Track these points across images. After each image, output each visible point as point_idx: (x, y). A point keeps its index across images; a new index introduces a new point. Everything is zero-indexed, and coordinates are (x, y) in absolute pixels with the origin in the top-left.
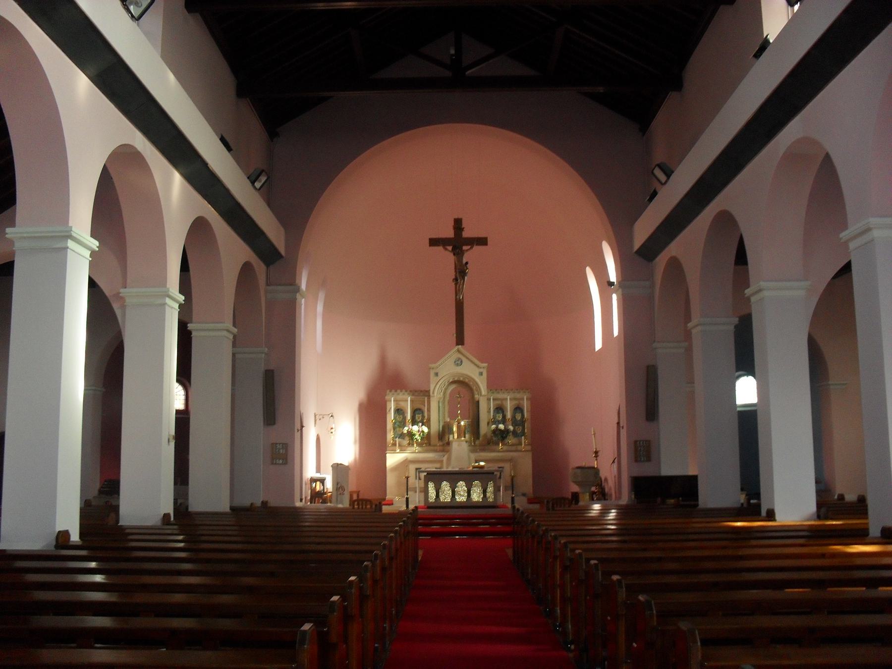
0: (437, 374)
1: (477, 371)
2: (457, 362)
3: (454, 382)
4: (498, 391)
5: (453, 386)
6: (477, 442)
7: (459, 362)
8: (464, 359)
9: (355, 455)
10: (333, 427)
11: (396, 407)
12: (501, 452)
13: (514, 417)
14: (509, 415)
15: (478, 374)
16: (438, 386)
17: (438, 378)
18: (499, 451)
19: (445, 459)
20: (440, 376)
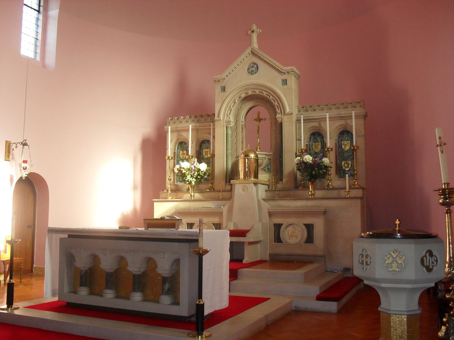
0: (224, 89)
1: (280, 78)
2: (251, 69)
3: (247, 98)
4: (321, 107)
5: (249, 105)
6: (280, 186)
7: (254, 69)
8: (261, 64)
9: (135, 204)
10: (23, 171)
11: (178, 139)
12: (312, 199)
13: (339, 146)
14: (329, 143)
15: (280, 82)
16: (225, 105)
17: (225, 94)
18: (308, 199)
19: (225, 210)
20: (228, 90)
